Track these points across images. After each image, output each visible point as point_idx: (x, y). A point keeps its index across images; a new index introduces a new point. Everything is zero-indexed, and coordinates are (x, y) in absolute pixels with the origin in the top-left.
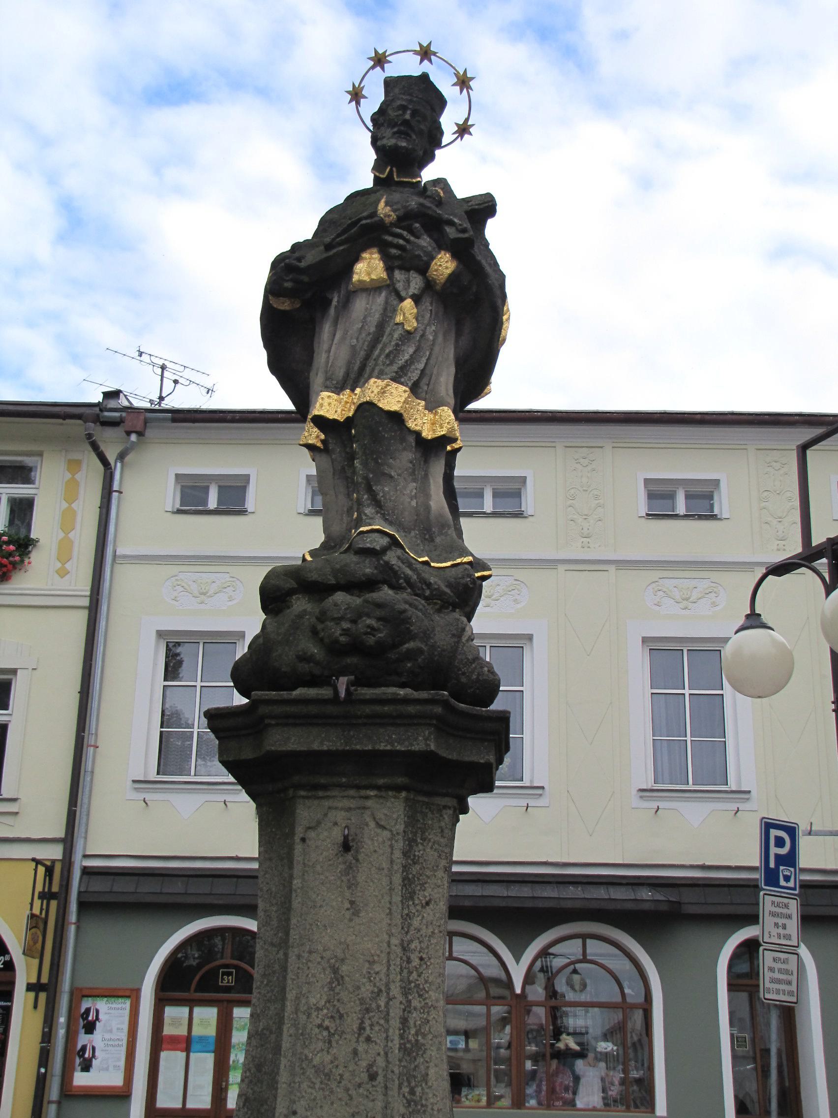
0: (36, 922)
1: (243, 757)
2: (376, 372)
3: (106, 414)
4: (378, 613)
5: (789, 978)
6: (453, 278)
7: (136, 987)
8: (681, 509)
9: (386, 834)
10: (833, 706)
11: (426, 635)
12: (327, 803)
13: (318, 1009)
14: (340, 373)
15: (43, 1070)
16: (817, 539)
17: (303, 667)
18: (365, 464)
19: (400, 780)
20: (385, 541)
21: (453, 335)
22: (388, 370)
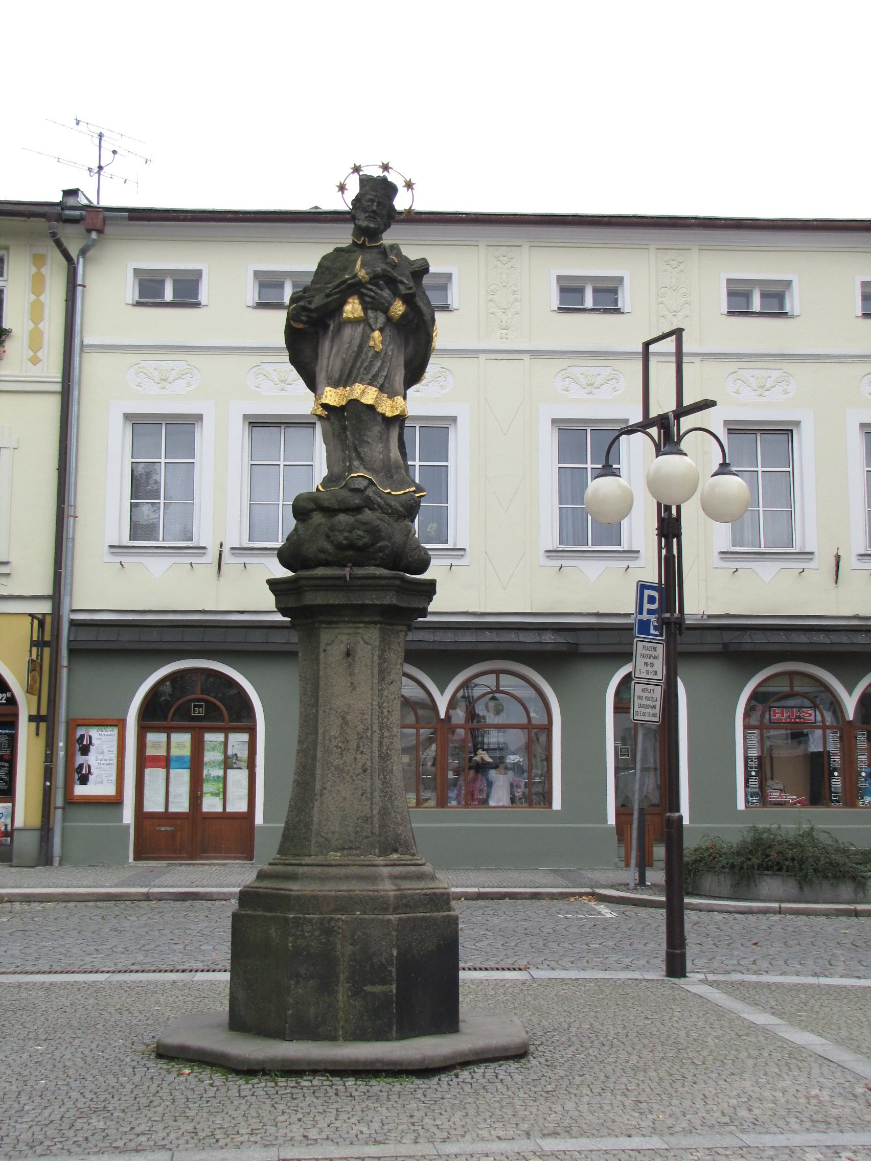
0: (34, 666)
1: (290, 606)
2: (359, 379)
3: (67, 212)
4: (364, 527)
5: (654, 703)
6: (404, 316)
7: (122, 718)
8: (589, 303)
9: (369, 647)
10: (656, 532)
11: (390, 538)
12: (337, 631)
13: (335, 738)
14: (336, 375)
15: (48, 784)
16: (653, 414)
17: (322, 556)
18: (353, 435)
19: (377, 619)
20: (365, 483)
21: (403, 349)
22: (365, 378)
